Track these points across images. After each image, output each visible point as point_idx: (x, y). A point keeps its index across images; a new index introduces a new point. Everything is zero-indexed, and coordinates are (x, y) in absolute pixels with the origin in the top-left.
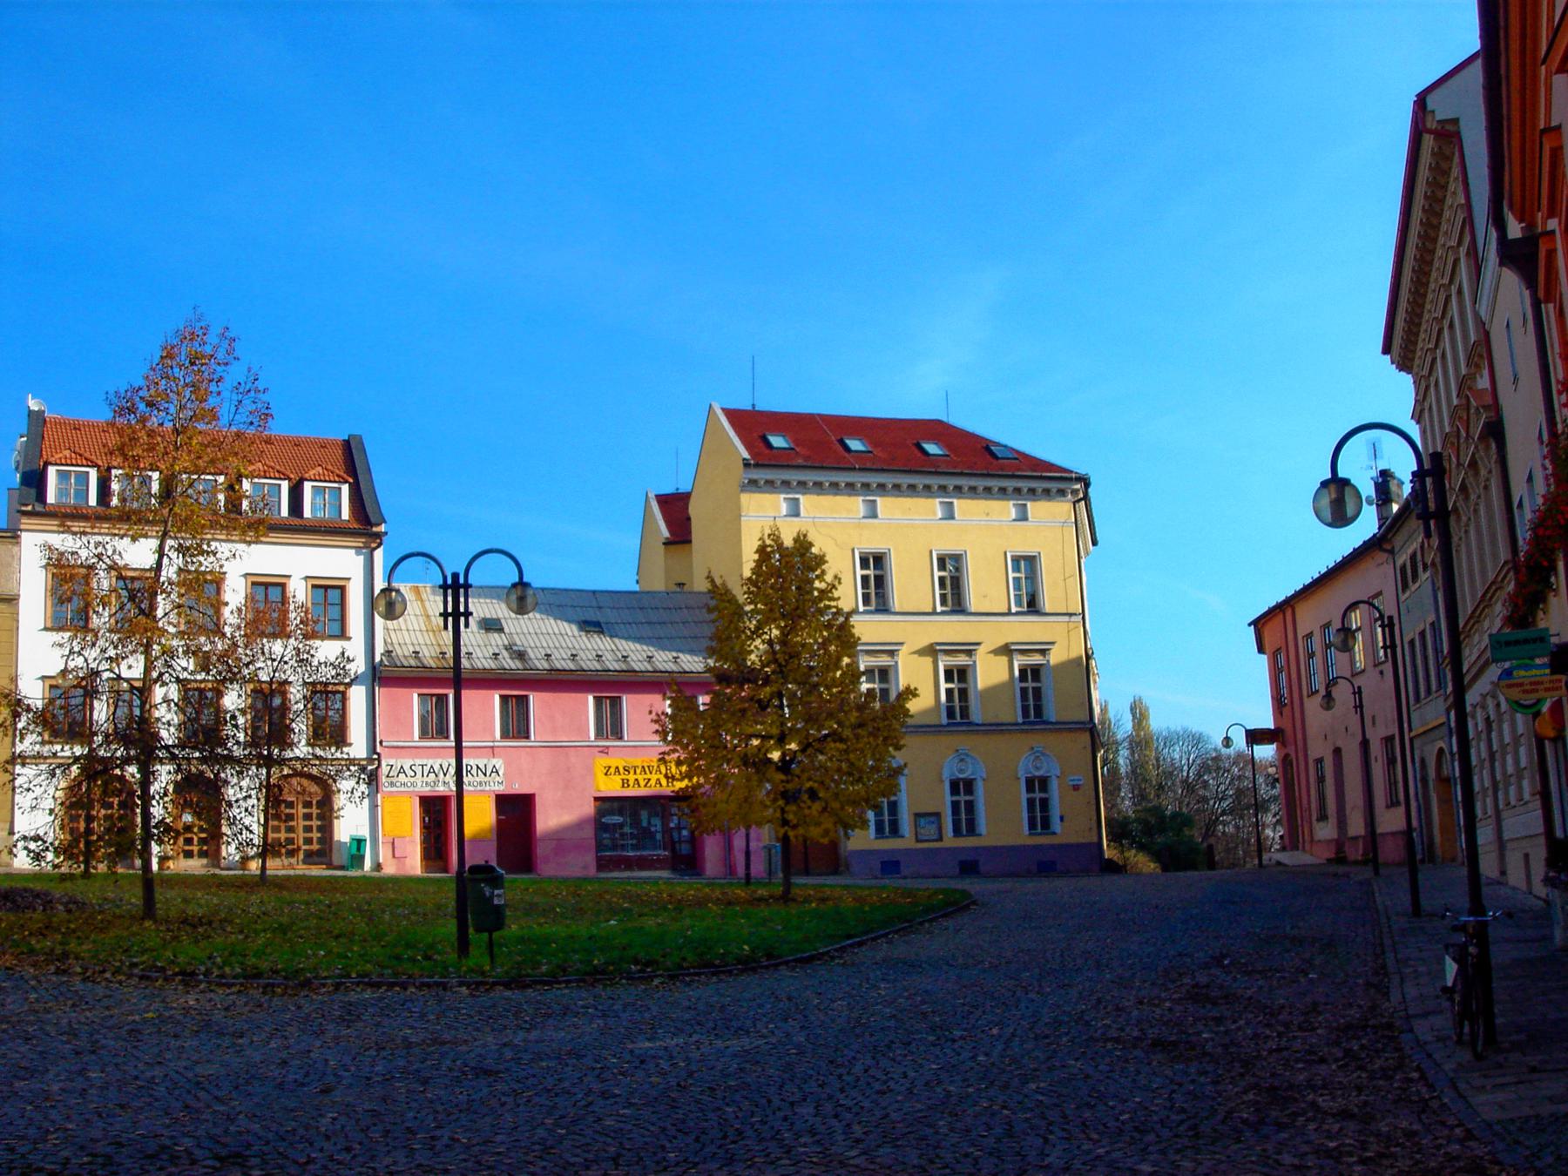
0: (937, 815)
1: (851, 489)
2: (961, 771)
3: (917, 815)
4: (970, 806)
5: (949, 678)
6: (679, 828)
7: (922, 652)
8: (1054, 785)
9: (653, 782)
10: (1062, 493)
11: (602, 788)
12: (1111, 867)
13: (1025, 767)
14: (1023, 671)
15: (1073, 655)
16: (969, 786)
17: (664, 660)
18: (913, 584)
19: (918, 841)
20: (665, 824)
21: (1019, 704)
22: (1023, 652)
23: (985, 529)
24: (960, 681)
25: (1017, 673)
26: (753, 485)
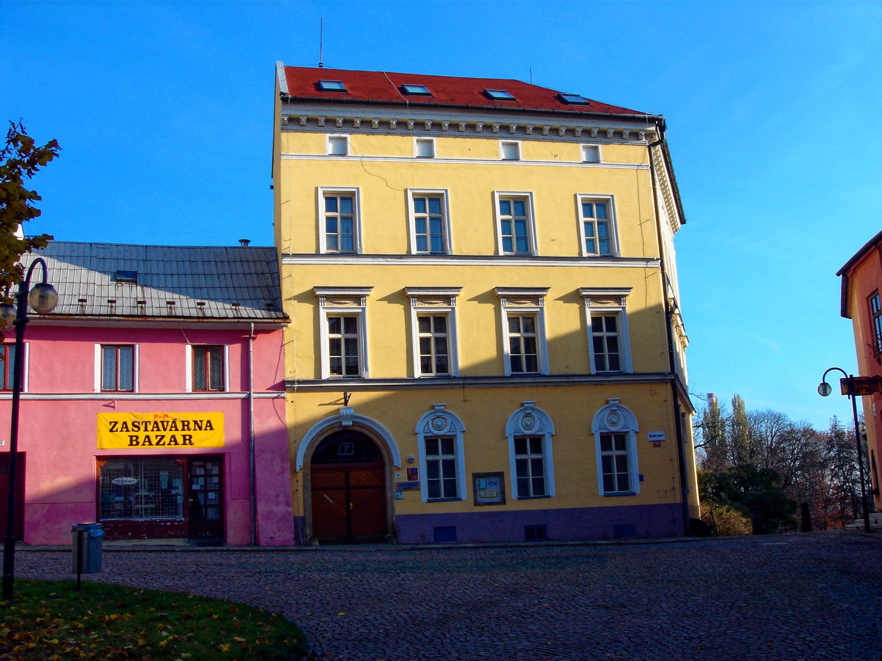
0: (500, 475)
1: (402, 128)
2: (527, 427)
3: (476, 476)
4: (538, 465)
5: (514, 328)
6: (205, 490)
7: (482, 299)
8: (633, 442)
9: (167, 440)
10: (635, 136)
11: (106, 446)
12: (702, 529)
13: (600, 421)
14: (596, 320)
15: (652, 302)
16: (537, 443)
17: (186, 306)
18: (385, 224)
19: (476, 504)
20: (188, 483)
21: (592, 354)
22: (421, 298)
23: (554, 173)
24: (347, 331)
25: (589, 322)
26: (294, 123)
